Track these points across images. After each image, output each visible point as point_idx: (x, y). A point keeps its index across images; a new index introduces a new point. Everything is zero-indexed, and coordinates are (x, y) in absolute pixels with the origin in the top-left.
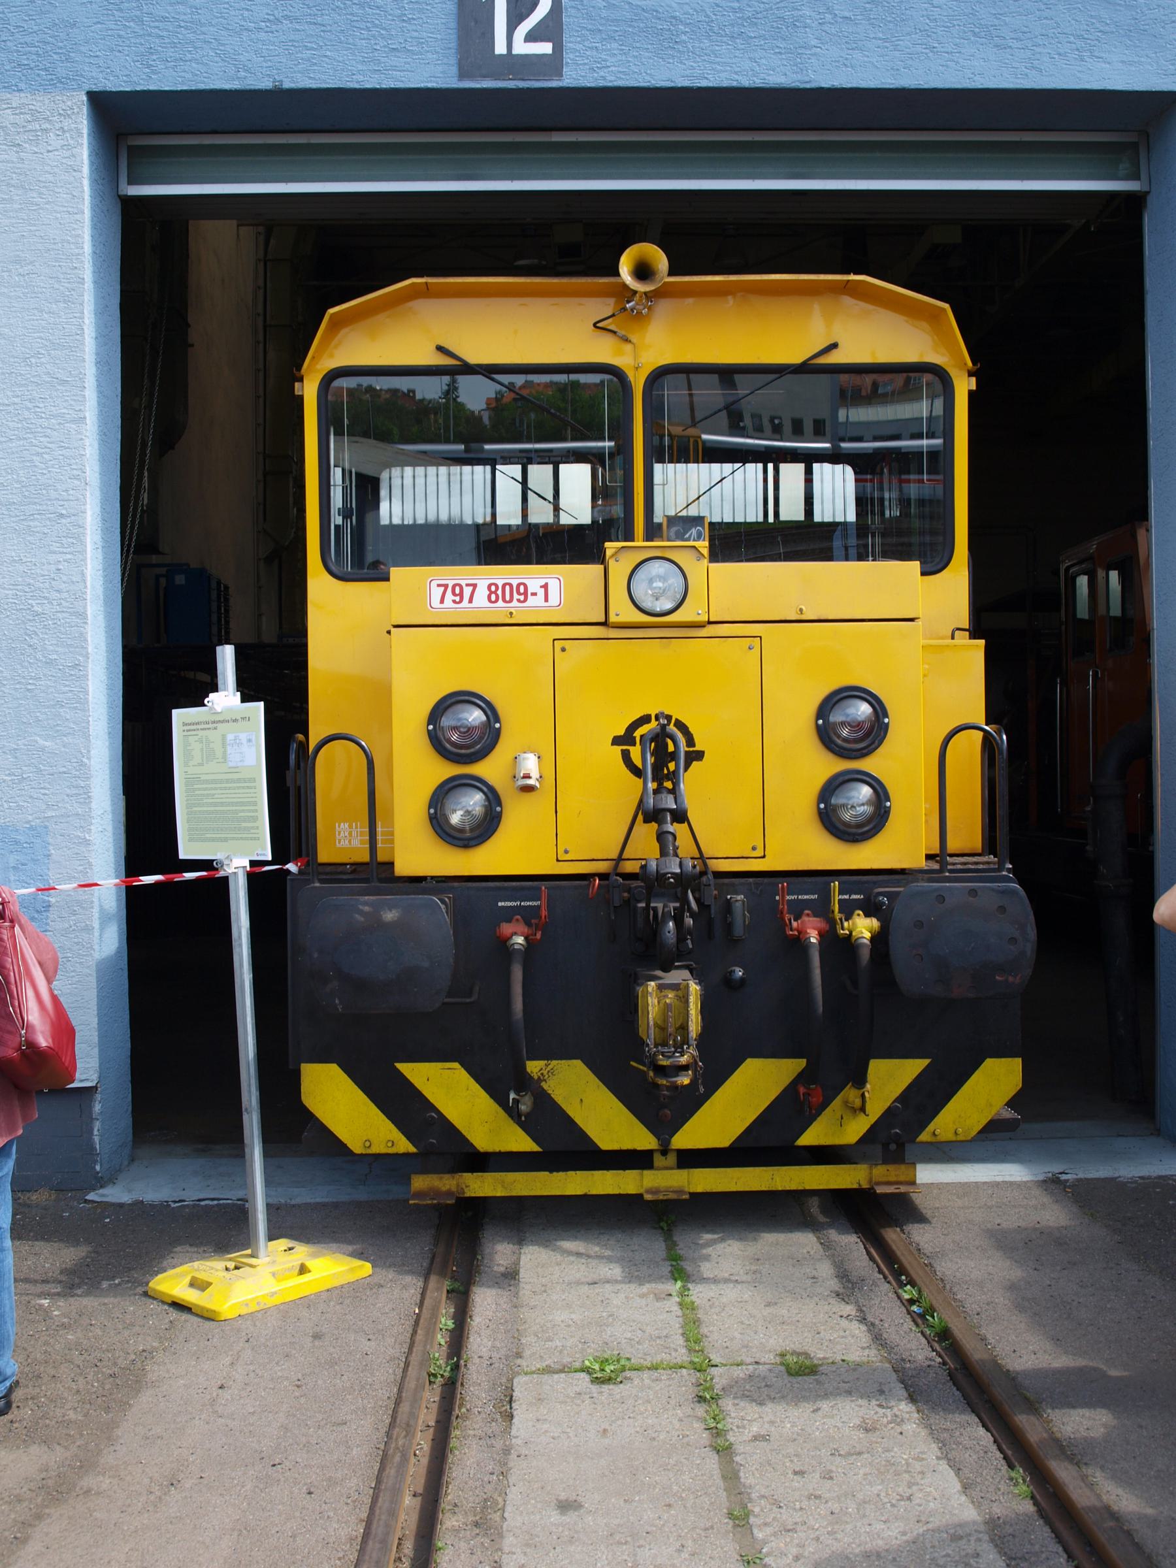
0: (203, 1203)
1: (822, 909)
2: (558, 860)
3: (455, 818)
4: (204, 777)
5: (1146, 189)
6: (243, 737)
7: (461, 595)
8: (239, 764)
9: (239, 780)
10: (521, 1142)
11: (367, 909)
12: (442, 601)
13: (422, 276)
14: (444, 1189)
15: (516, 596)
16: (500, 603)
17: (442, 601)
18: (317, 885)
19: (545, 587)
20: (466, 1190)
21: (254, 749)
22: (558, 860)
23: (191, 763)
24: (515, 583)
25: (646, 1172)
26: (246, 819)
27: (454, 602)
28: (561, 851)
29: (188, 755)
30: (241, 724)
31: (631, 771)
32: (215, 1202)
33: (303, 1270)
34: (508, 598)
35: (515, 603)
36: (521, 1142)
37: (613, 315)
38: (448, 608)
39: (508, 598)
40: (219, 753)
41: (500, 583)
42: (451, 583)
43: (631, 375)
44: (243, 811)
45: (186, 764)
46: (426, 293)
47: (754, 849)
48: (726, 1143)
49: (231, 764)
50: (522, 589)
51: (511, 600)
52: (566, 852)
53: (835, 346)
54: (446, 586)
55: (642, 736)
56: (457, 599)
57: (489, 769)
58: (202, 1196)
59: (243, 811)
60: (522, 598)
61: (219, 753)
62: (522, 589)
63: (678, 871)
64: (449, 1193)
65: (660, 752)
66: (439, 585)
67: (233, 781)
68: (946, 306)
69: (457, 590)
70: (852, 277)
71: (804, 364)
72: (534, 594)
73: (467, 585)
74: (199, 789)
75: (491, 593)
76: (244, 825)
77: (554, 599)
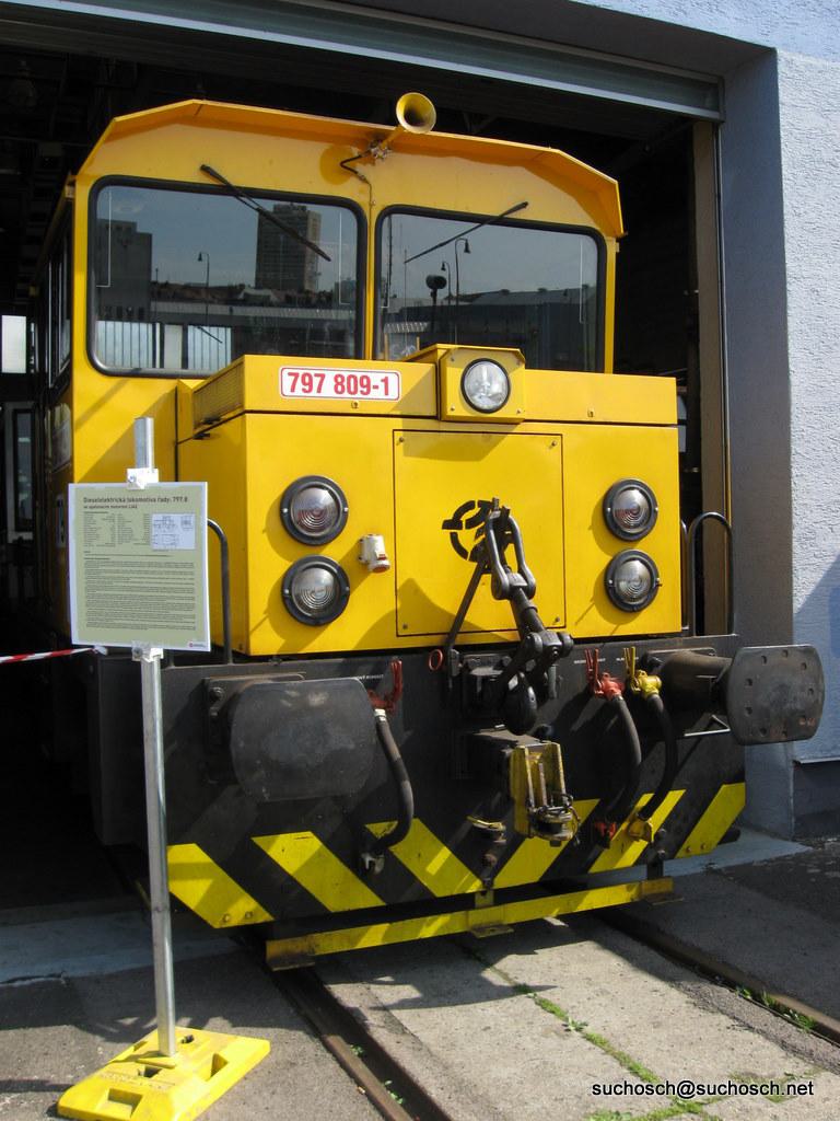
0: (17, 984)
1: (614, 669)
2: (398, 636)
3: (310, 601)
4: (113, 559)
5: (722, 119)
6: (177, 518)
7: (310, 384)
8: (169, 547)
9: (168, 564)
10: (368, 899)
11: (294, 694)
12: (293, 389)
13: (201, 99)
14: (298, 951)
15: (360, 388)
16: (346, 394)
17: (293, 389)
18: (173, 667)
19: (385, 381)
20: (316, 949)
21: (192, 533)
22: (398, 636)
23: (95, 543)
24: (359, 375)
25: (471, 912)
26: (181, 607)
27: (304, 390)
28: (400, 627)
29: (90, 534)
30: (173, 504)
31: (458, 552)
32: (27, 982)
33: (217, 1064)
34: (352, 389)
35: (359, 395)
36: (368, 899)
37: (360, 157)
38: (297, 396)
39: (352, 389)
40: (139, 533)
41: (346, 375)
42: (301, 372)
43: (366, 210)
44: (173, 598)
45: (88, 542)
46: (193, 119)
47: (557, 620)
48: (535, 878)
49: (155, 547)
50: (365, 382)
51: (355, 392)
52: (405, 627)
53: (524, 205)
54: (296, 375)
55: (467, 520)
56: (307, 388)
57: (336, 551)
58: (10, 976)
59: (173, 598)
60: (365, 390)
61: (139, 533)
62: (365, 382)
63: (559, 643)
64: (303, 956)
65: (489, 533)
66: (290, 374)
67: (159, 565)
68: (616, 182)
69: (307, 379)
70: (550, 149)
71: (502, 216)
72: (376, 387)
73: (316, 375)
74: (106, 571)
75: (337, 384)
76: (172, 612)
77: (393, 393)
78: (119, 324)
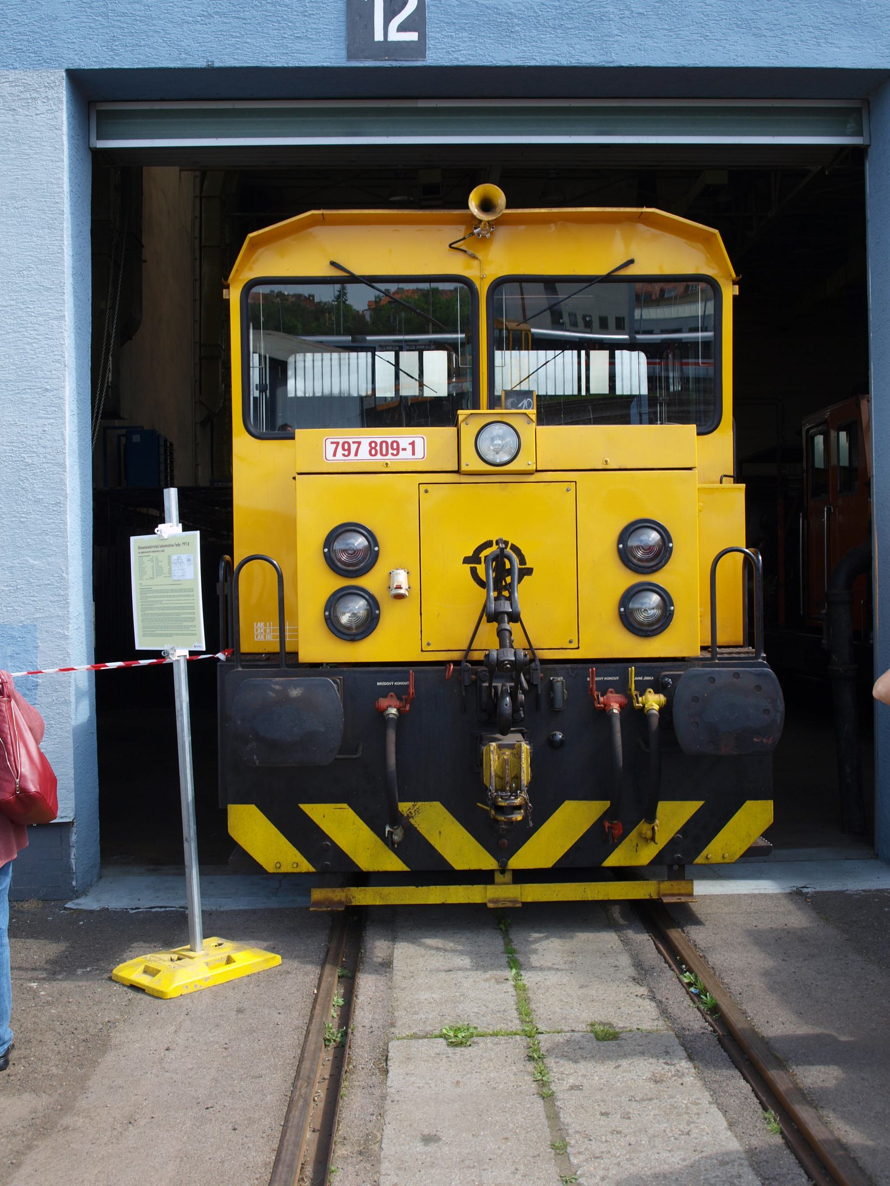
0: (153, 910)
1: (622, 688)
2: (422, 651)
3: (345, 619)
4: (154, 588)
5: (867, 143)
6: (184, 557)
7: (349, 450)
8: (181, 578)
9: (181, 590)
10: (394, 864)
11: (277, 687)
12: (335, 455)
13: (319, 209)
14: (336, 899)
15: (390, 451)
16: (379, 456)
17: (335, 455)
18: (240, 669)
19: (413, 444)
20: (353, 900)
21: (192, 567)
22: (422, 651)
23: (144, 577)
24: (390, 441)
25: (489, 887)
26: (186, 620)
27: (344, 455)
28: (424, 643)
29: (142, 571)
30: (182, 547)
31: (477, 583)
32: (163, 909)
34: (384, 452)
35: (390, 456)
36: (394, 864)
37: (464, 239)
38: (339, 460)
39: (384, 452)
40: (166, 570)
41: (378, 441)
42: (341, 441)
43: (477, 284)
44: (184, 613)
45: (141, 578)
46: (323, 221)
47: (571, 642)
48: (549, 865)
49: (175, 578)
50: (395, 446)
51: (387, 454)
52: (429, 644)
53: (632, 262)
54: (338, 443)
55: (486, 557)
56: (346, 453)
57: (370, 582)
58: (153, 905)
59: (184, 613)
60: (395, 452)
61: (166, 570)
62: (395, 446)
63: (513, 659)
64: (340, 903)
65: (500, 569)
66: (332, 443)
67: (176, 591)
68: (716, 232)
69: (346, 447)
70: (645, 210)
71: (609, 275)
72: (404, 449)
73: (354, 442)
74: (151, 597)
75: (372, 448)
76: (185, 624)
77: (419, 453)
78: (515, 353)
